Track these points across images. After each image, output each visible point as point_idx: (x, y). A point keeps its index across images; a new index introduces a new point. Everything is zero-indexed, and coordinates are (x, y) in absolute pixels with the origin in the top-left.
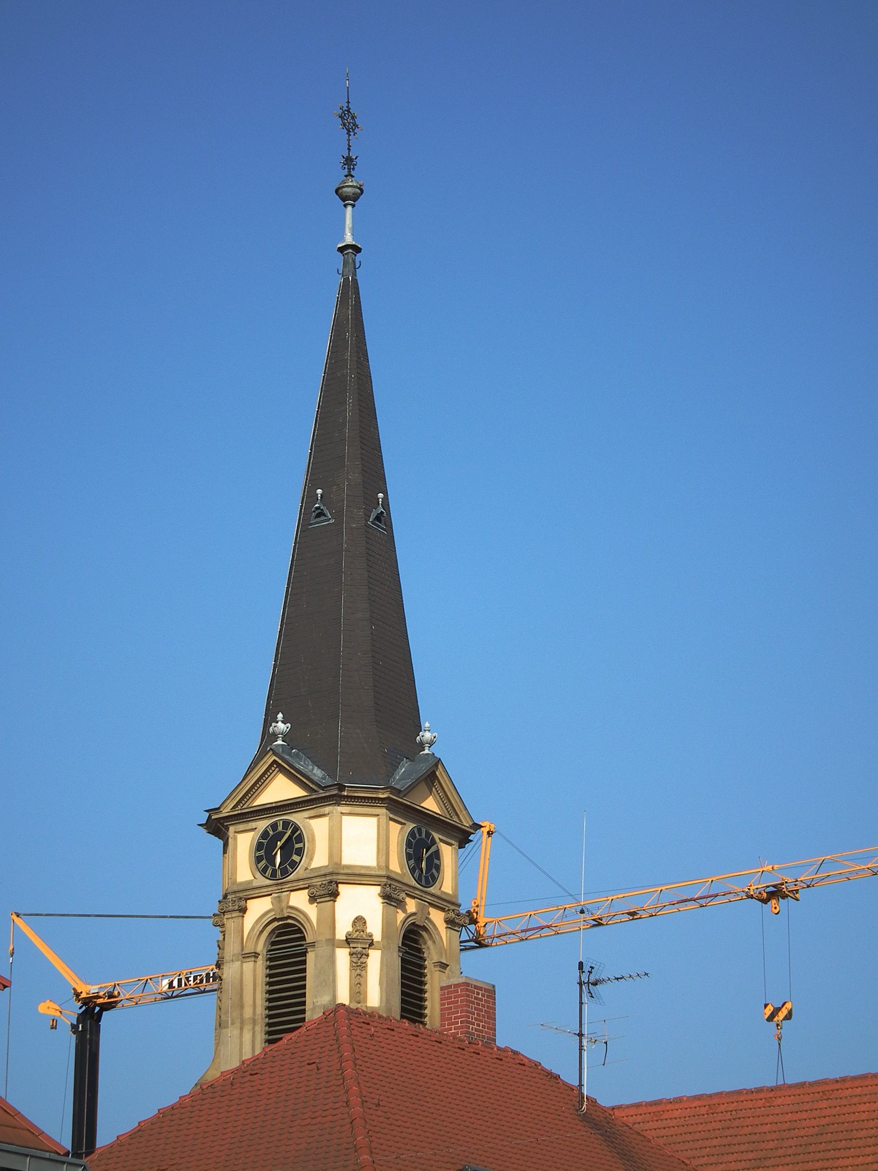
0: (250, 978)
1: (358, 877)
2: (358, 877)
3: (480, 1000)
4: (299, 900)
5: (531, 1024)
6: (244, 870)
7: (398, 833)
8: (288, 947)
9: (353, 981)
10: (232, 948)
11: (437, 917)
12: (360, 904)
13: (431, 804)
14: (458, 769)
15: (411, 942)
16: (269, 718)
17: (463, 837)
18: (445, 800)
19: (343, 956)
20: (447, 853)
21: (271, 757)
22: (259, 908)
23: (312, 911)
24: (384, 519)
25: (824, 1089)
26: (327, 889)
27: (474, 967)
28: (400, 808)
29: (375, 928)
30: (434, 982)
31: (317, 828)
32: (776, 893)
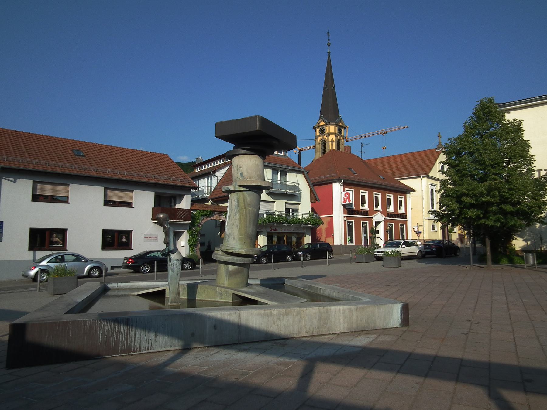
0: (319, 147)
1: (332, 133)
2: (332, 133)
3: (349, 148)
4: (325, 137)
5: (355, 151)
6: (318, 134)
7: (337, 128)
8: (324, 142)
9: (332, 146)
10: (317, 143)
11: (342, 138)
12: (332, 137)
13: (341, 124)
14: (343, 120)
15: (339, 141)
16: (320, 115)
17: (344, 128)
18: (342, 124)
19: (330, 143)
20: (343, 130)
21: (321, 119)
22: (320, 138)
23: (326, 138)
24: (334, 88)
25: (391, 157)
26: (328, 135)
27: (346, 144)
28: (337, 125)
29: (334, 140)
30: (341, 146)
31: (327, 128)
32: (384, 133)
